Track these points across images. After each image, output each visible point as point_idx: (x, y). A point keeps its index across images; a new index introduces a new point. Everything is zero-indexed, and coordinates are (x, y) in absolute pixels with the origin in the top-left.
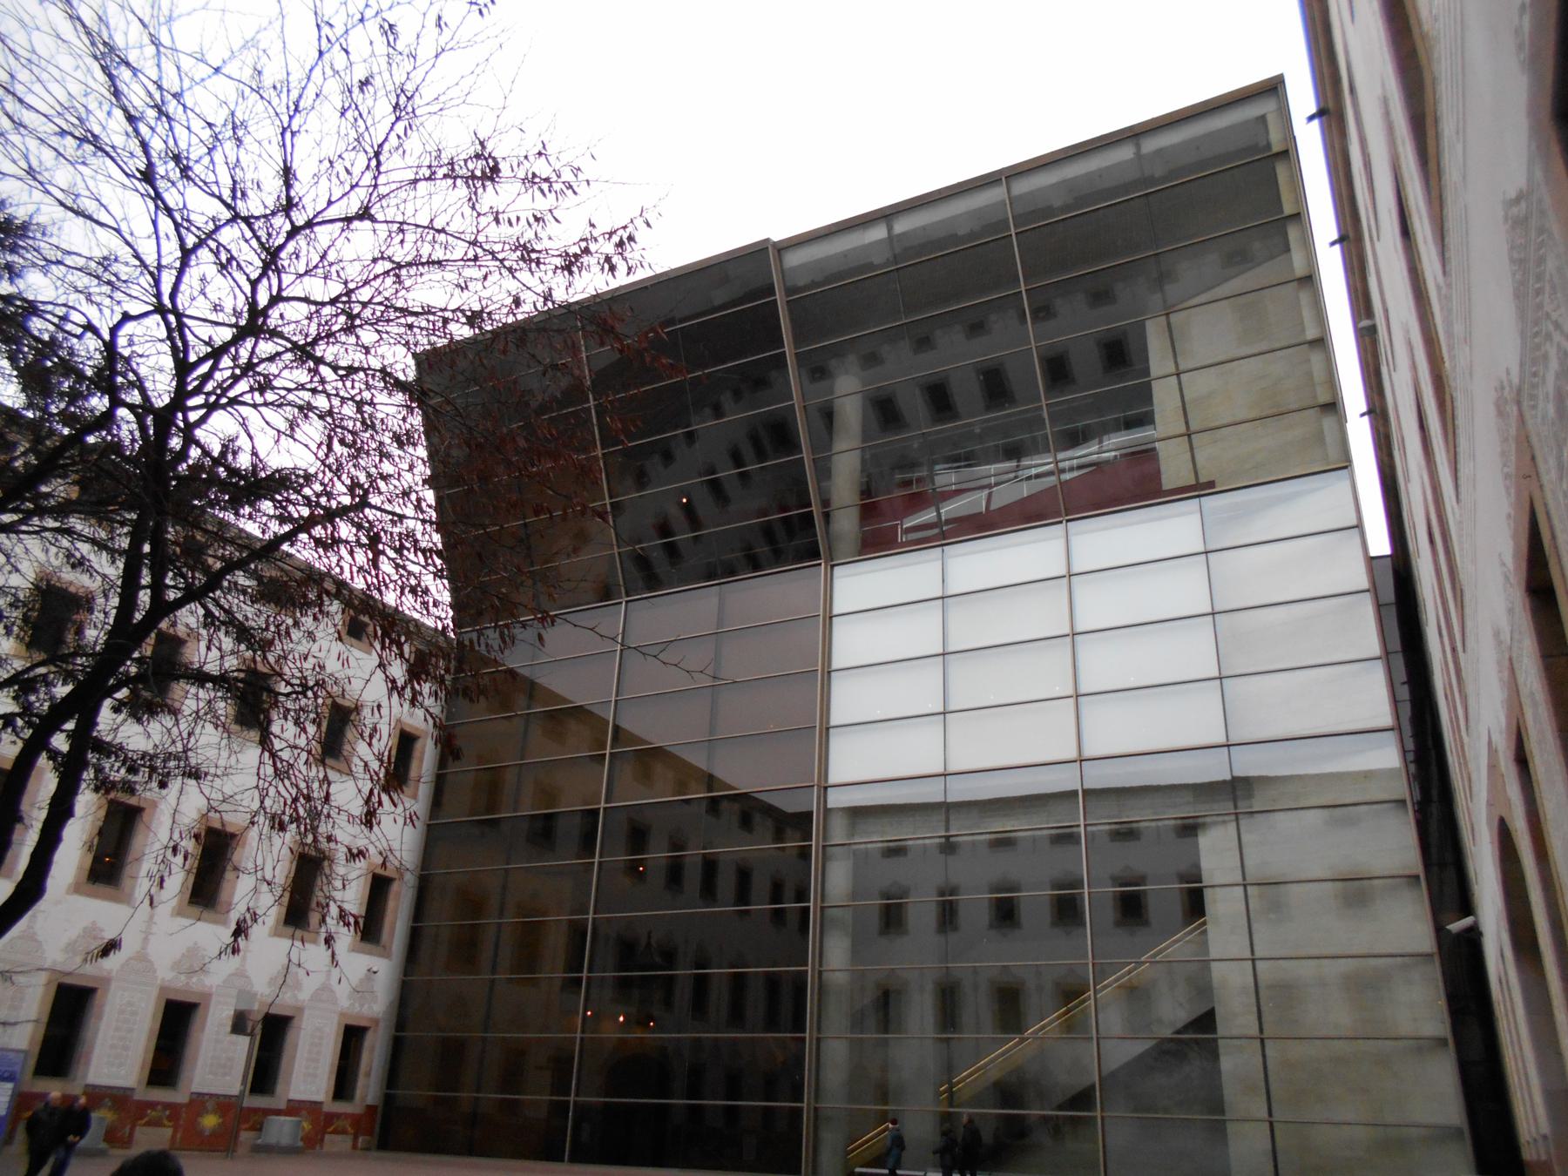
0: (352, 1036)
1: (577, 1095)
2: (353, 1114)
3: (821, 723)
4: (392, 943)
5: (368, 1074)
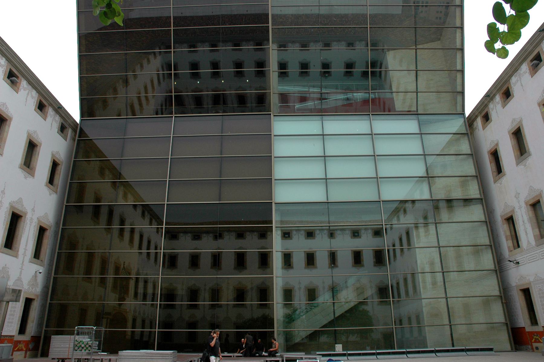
1: (156, 331)
2: (26, 341)
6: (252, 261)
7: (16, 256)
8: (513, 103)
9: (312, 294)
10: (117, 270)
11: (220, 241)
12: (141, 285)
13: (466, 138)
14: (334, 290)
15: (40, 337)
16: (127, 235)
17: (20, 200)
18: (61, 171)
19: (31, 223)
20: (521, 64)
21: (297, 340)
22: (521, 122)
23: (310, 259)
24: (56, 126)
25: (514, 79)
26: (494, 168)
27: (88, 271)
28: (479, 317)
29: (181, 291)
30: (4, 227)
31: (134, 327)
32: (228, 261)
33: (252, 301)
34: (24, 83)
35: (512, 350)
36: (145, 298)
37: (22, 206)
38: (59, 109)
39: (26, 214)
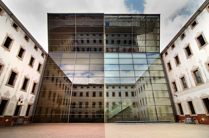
6: (97, 94)
7: (13, 87)
8: (175, 49)
9: (94, 104)
10: (58, 97)
11: (89, 89)
12: (66, 101)
13: (160, 59)
14: (121, 103)
15: (33, 117)
16: (62, 86)
17: (28, 75)
18: (42, 67)
19: (7, 69)
20: (178, 37)
21: (110, 117)
22: (178, 54)
23: (114, 94)
24: (40, 54)
25: (175, 42)
26: (169, 68)
27: (50, 96)
28: (164, 112)
29: (77, 102)
31: (63, 113)
32: (91, 94)
33: (97, 106)
34: (30, 40)
35: (176, 122)
36: (67, 105)
38: (41, 49)
39: (4, 66)
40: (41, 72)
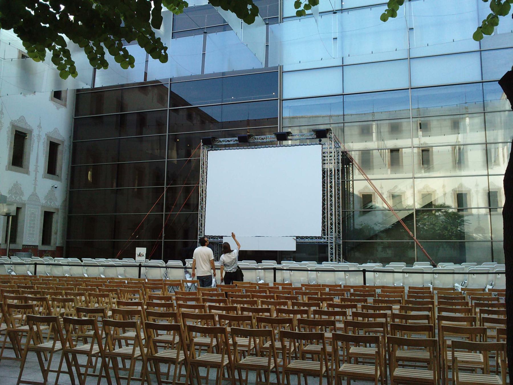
0: (48, 216)
3: (280, 71)
4: (61, 174)
5: (56, 233)
30: (8, 146)
37: (26, 124)
39: (31, 132)
40: (67, 103)
